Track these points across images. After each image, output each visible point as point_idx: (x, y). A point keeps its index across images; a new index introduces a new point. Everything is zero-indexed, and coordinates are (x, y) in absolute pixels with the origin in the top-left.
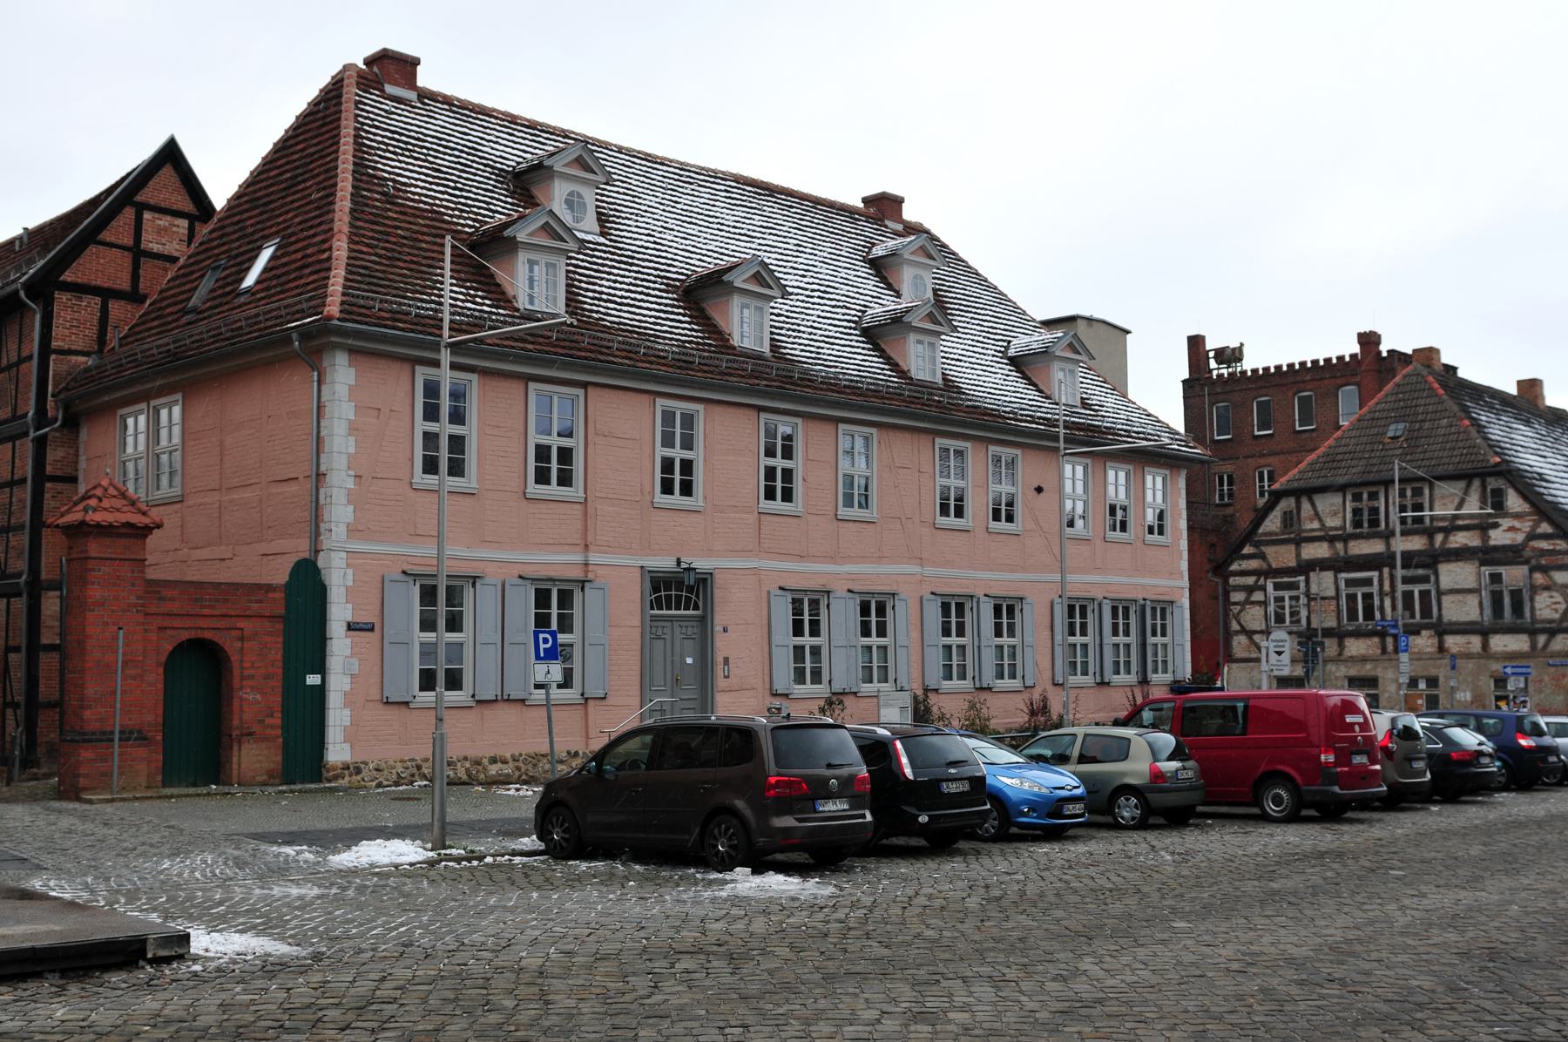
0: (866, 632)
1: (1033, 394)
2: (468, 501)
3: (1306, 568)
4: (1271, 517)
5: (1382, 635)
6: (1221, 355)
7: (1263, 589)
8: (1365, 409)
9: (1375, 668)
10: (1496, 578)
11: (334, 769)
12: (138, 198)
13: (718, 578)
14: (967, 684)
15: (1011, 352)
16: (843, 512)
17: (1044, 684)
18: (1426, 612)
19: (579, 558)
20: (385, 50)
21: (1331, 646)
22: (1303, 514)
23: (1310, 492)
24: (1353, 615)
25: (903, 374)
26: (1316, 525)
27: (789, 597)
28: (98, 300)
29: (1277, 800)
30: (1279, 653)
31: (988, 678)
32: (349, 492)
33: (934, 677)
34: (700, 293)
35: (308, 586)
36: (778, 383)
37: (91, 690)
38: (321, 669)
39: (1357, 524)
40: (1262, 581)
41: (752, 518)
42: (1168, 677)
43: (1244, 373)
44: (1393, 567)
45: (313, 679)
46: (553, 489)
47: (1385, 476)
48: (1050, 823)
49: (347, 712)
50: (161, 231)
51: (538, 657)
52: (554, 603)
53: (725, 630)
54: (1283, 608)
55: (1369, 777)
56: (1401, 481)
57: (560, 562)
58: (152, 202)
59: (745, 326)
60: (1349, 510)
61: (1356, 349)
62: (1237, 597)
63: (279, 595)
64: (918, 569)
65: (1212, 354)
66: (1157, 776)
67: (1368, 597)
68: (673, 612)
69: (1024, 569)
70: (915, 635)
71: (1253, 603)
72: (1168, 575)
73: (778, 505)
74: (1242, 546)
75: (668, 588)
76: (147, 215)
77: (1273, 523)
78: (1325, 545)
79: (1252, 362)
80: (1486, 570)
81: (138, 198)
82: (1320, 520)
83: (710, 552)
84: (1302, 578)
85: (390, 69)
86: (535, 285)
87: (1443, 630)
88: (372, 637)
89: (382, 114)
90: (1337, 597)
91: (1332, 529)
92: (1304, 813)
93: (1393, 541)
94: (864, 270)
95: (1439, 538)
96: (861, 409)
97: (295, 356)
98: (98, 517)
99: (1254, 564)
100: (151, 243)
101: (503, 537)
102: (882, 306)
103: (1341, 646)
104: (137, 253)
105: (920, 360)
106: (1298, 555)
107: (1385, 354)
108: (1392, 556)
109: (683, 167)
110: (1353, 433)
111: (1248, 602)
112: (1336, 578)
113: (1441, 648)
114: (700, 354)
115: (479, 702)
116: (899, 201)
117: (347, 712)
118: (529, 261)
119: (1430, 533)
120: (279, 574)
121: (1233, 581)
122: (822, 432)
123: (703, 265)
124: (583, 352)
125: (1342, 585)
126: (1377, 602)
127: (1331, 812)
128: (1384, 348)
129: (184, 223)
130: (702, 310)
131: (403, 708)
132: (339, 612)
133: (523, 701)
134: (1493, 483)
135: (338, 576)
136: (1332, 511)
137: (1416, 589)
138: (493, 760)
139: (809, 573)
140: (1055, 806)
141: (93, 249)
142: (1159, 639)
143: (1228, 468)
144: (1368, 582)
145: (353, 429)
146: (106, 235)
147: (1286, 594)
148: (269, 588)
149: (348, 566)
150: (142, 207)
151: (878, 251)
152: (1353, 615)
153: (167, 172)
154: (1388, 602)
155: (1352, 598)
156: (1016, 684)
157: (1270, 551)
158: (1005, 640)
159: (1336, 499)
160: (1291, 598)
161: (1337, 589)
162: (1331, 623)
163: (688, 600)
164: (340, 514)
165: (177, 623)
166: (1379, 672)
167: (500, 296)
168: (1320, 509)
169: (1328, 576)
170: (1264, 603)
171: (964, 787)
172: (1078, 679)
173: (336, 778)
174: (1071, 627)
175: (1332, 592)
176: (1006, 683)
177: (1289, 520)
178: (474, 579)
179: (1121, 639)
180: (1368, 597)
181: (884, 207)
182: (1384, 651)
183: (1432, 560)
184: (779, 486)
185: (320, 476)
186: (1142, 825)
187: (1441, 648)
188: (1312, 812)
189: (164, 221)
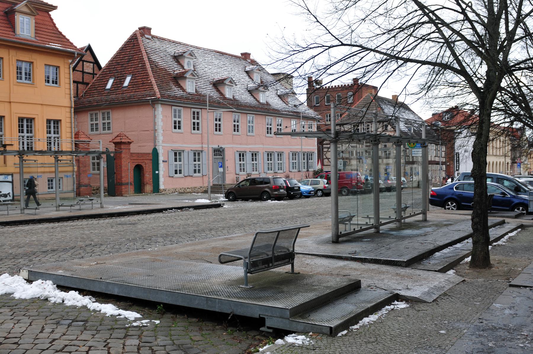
0: (253, 161)
1: (284, 105)
2: (182, 135)
13: (226, 150)
14: (272, 172)
15: (278, 94)
16: (249, 134)
17: (287, 172)
19: (201, 146)
25: (258, 101)
29: (345, 192)
31: (277, 170)
32: (162, 134)
33: (238, 171)
34: (218, 84)
35: (155, 153)
36: (235, 105)
37: (123, 175)
38: (158, 170)
41: (231, 136)
42: (312, 170)
45: (157, 172)
46: (196, 131)
48: (308, 195)
50: (88, 67)
52: (197, 155)
55: (361, 188)
59: (228, 93)
62: (325, 150)
66: (325, 187)
69: (283, 145)
70: (262, 161)
73: (236, 133)
76: (85, 63)
79: (17, 296)
83: (224, 144)
85: (145, 31)
86: (190, 86)
88: (167, 163)
89: (144, 43)
94: (245, 74)
97: (149, 104)
98: (123, 141)
101: (188, 141)
102: (251, 85)
105: (263, 98)
109: (204, 49)
111: (328, 151)
114: (217, 99)
116: (249, 54)
120: (150, 151)
123: (217, 77)
124: (197, 101)
127: (355, 193)
129: (92, 64)
130: (218, 89)
132: (161, 158)
135: (161, 151)
139: (242, 148)
140: (309, 192)
142: (311, 161)
145: (162, 120)
148: (149, 154)
150: (84, 61)
151: (248, 69)
156: (282, 171)
158: (242, 162)
165: (135, 161)
167: (184, 90)
171: (297, 188)
172: (294, 170)
176: (280, 171)
179: (294, 161)
184: (236, 128)
185: (156, 130)
186: (322, 196)
189: (88, 64)
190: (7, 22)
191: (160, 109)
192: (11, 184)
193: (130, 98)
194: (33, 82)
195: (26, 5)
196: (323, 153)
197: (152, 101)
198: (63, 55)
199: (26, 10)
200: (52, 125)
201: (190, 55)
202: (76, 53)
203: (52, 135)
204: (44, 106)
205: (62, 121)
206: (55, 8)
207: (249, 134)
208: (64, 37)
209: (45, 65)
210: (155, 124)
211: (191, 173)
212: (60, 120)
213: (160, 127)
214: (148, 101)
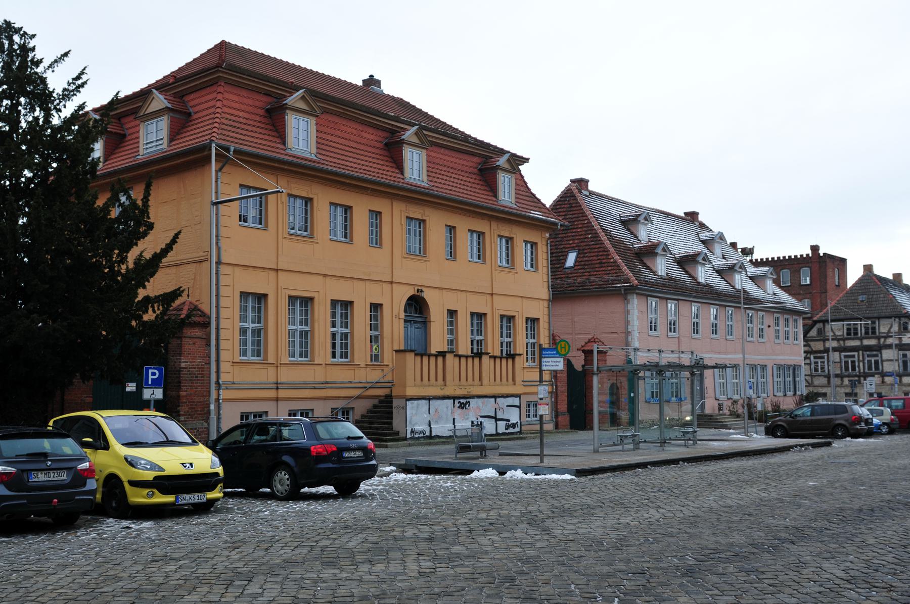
10: (905, 356)
16: (728, 337)
18: (877, 368)
24: (847, 369)
39: (849, 334)
61: (810, 252)
67: (853, 362)
80: (901, 353)
85: (581, 183)
87: (883, 375)
90: (841, 362)
95: (882, 340)
96: (705, 298)
103: (842, 381)
113: (883, 382)
116: (587, 182)
119: (879, 338)
126: (857, 364)
128: (821, 252)
134: (903, 320)
137: (873, 359)
144: (853, 356)
147: (819, 361)
152: (847, 369)
155: (846, 363)
157: (812, 344)
162: (838, 372)
167: (655, 273)
169: (837, 354)
177: (820, 332)
180: (853, 362)
181: (692, 217)
183: (879, 348)
187: (883, 382)
190: (271, 128)
191: (635, 304)
192: (518, 409)
193: (583, 284)
194: (312, 233)
195: (303, 98)
197: (625, 290)
198: (533, 224)
199: (302, 105)
200: (338, 311)
201: (646, 219)
202: (232, 149)
203: (339, 330)
204: (328, 279)
205: (384, 307)
206: (527, 160)
207: (728, 337)
208: (539, 200)
209: (331, 204)
210: (627, 323)
212: (381, 305)
213: (636, 328)
214: (619, 289)
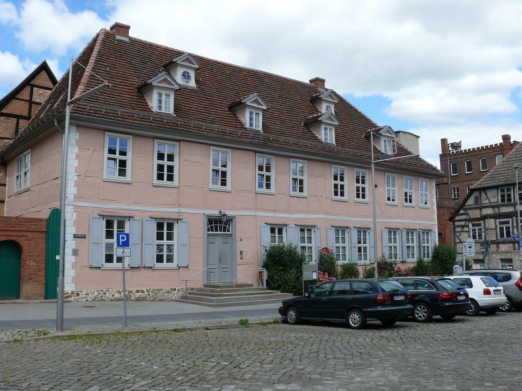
2: (128, 186)
3: (484, 218)
4: (470, 199)
5: (514, 243)
6: (453, 145)
7: (468, 226)
8: (505, 159)
9: (511, 255)
11: (68, 293)
12: (31, 83)
20: (116, 23)
21: (493, 247)
22: (482, 198)
23: (484, 189)
24: (502, 235)
26: (487, 201)
27: (269, 227)
28: (15, 119)
30: (470, 247)
35: (56, 216)
39: (503, 200)
40: (467, 223)
43: (461, 151)
44: (517, 216)
47: (513, 182)
49: (73, 271)
50: (40, 95)
51: (118, 245)
52: (165, 228)
53: (241, 240)
54: (476, 233)
56: (519, 184)
57: (167, 211)
58: (36, 84)
60: (499, 195)
61: (501, 141)
63: (44, 223)
64: (325, 216)
65: (450, 145)
67: (508, 228)
68: (218, 232)
71: (464, 231)
72: (431, 220)
74: (459, 210)
75: (216, 222)
76: (35, 89)
77: (471, 201)
78: (491, 209)
79: (464, 147)
81: (31, 83)
82: (489, 199)
83: (234, 209)
84: (482, 222)
90: (496, 229)
91: (493, 203)
92: (481, 312)
93: (516, 207)
99: (464, 217)
100: (36, 99)
101: (142, 199)
103: (498, 247)
104: (31, 102)
106: (481, 213)
107: (512, 143)
108: (516, 213)
110: (502, 167)
112: (495, 222)
115: (131, 268)
117: (73, 271)
118: (158, 93)
120: (45, 214)
121: (456, 223)
122: (283, 162)
125: (498, 224)
126: (511, 230)
128: (512, 141)
131: (98, 269)
132: (70, 230)
133: (151, 267)
135: (70, 216)
136: (494, 197)
138: (138, 291)
141: (14, 102)
143: (457, 186)
146: (19, 96)
147: (477, 228)
148: (40, 220)
149: (74, 212)
152: (502, 235)
153: (44, 74)
154: (515, 230)
155: (501, 229)
157: (470, 212)
159: (495, 191)
160: (478, 229)
161: (496, 226)
162: (494, 238)
163: (225, 228)
164: (71, 190)
166: (513, 257)
168: (488, 195)
169: (492, 220)
170: (469, 232)
173: (68, 297)
174: (390, 239)
175: (494, 227)
177: (477, 200)
178: (130, 218)
180: (508, 228)
182: (514, 249)
188: (439, 317)
189: (41, 91)
196: (454, 235)
211: (150, 259)
